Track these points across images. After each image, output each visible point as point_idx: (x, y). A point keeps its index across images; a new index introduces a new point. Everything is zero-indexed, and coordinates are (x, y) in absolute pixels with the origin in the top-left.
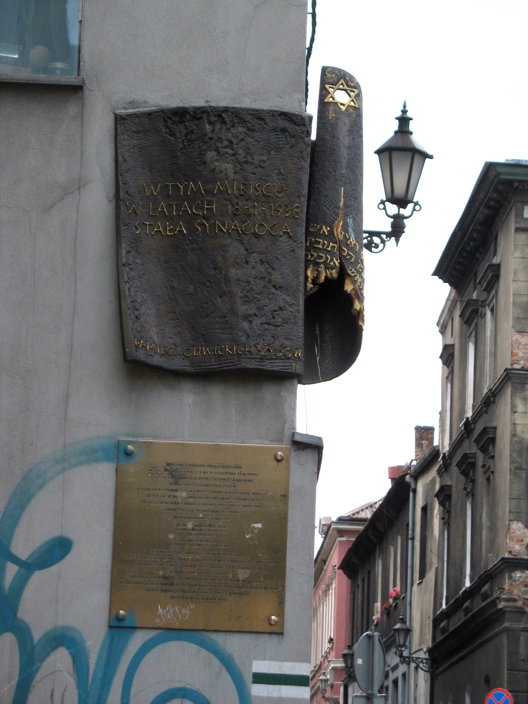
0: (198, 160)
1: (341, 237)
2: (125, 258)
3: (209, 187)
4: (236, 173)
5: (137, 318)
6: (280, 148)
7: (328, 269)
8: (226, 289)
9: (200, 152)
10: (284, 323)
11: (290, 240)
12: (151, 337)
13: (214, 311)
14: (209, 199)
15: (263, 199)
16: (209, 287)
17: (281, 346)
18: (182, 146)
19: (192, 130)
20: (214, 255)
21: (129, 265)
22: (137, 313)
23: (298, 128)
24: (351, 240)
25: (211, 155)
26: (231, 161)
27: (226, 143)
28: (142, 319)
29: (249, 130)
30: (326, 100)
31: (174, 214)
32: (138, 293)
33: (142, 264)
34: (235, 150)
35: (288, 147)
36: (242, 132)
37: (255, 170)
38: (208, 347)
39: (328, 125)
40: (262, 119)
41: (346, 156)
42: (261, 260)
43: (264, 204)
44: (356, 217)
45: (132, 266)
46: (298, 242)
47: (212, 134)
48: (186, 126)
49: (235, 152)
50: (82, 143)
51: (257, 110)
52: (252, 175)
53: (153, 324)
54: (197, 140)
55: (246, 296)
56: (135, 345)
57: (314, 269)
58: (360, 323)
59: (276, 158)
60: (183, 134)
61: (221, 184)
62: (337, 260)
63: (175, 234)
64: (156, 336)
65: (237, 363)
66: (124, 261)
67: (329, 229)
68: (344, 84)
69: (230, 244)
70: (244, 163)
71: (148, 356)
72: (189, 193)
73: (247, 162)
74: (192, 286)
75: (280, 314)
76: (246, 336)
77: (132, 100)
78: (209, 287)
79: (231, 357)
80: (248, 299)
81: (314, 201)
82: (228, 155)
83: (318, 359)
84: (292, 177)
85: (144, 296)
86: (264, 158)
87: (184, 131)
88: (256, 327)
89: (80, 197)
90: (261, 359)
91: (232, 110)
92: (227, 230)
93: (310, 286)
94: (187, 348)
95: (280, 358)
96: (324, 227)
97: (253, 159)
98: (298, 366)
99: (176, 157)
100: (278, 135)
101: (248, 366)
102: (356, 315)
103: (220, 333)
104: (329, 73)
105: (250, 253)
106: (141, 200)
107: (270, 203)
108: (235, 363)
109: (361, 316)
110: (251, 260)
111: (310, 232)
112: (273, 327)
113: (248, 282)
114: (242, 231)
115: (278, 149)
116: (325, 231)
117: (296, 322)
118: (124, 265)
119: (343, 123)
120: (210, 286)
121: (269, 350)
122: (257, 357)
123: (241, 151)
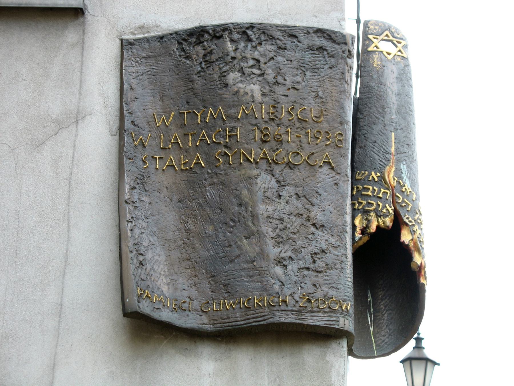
0: (218, 83)
1: (394, 183)
2: (128, 194)
3: (232, 111)
4: (263, 95)
5: (141, 263)
6: (318, 69)
7: (380, 216)
8: (254, 228)
9: (221, 74)
10: (328, 268)
11: (332, 171)
12: (159, 288)
13: (239, 255)
14: (232, 125)
15: (298, 124)
16: (232, 227)
17: (325, 296)
18: (199, 69)
19: (212, 50)
20: (239, 188)
21: (134, 203)
22: (141, 258)
23: (337, 46)
24: (406, 187)
25: (233, 76)
26: (258, 82)
27: (251, 62)
28: (149, 267)
29: (279, 48)
30: (369, 49)
31: (190, 145)
32: (144, 235)
33: (150, 203)
34: (263, 69)
35: (326, 67)
36: (271, 50)
37: (287, 92)
38: (231, 299)
39: (373, 73)
40: (295, 37)
41: (395, 102)
42: (297, 194)
43: (299, 130)
44: (411, 165)
45: (137, 205)
46: (342, 174)
47: (235, 54)
48: (204, 46)
49: (262, 72)
50: (81, 72)
51: (288, 27)
52: (283, 97)
53: (162, 273)
54: (217, 60)
55: (279, 236)
56: (138, 295)
57: (363, 218)
58: (422, 281)
59: (313, 79)
60: (201, 56)
61: (246, 108)
62: (391, 207)
63: (191, 168)
64: (166, 287)
65: (269, 316)
66: (127, 197)
67: (379, 174)
68: (389, 35)
69: (258, 175)
70: (274, 84)
71: (155, 310)
72: (207, 121)
73: (277, 83)
74: (212, 227)
75: (322, 258)
76: (280, 283)
77: (141, 24)
78: (232, 227)
79: (261, 310)
80: (281, 240)
81: (360, 148)
82: (254, 76)
83: (372, 329)
84: (332, 100)
85: (152, 240)
86: (298, 79)
87: (202, 52)
88: (292, 273)
89: (77, 132)
90: (300, 311)
91: (259, 26)
92: (254, 160)
93: (358, 235)
94: (205, 302)
95: (322, 310)
96: (373, 173)
97: (285, 80)
98: (346, 321)
99: (191, 81)
100: (315, 54)
101: (283, 320)
102: (417, 270)
103: (247, 282)
104: (372, 25)
105: (283, 186)
106: (150, 131)
107: (306, 129)
108: (265, 318)
109: (423, 273)
110: (284, 194)
111: (356, 180)
112: (313, 274)
113: (281, 220)
114: (273, 160)
115: (314, 70)
116: (375, 177)
117: (342, 268)
118: (126, 202)
119: (390, 70)
120: (235, 226)
121: (309, 301)
122: (294, 309)
123: (270, 71)
